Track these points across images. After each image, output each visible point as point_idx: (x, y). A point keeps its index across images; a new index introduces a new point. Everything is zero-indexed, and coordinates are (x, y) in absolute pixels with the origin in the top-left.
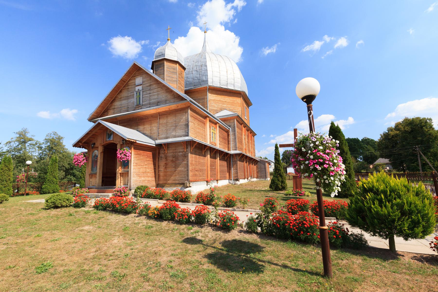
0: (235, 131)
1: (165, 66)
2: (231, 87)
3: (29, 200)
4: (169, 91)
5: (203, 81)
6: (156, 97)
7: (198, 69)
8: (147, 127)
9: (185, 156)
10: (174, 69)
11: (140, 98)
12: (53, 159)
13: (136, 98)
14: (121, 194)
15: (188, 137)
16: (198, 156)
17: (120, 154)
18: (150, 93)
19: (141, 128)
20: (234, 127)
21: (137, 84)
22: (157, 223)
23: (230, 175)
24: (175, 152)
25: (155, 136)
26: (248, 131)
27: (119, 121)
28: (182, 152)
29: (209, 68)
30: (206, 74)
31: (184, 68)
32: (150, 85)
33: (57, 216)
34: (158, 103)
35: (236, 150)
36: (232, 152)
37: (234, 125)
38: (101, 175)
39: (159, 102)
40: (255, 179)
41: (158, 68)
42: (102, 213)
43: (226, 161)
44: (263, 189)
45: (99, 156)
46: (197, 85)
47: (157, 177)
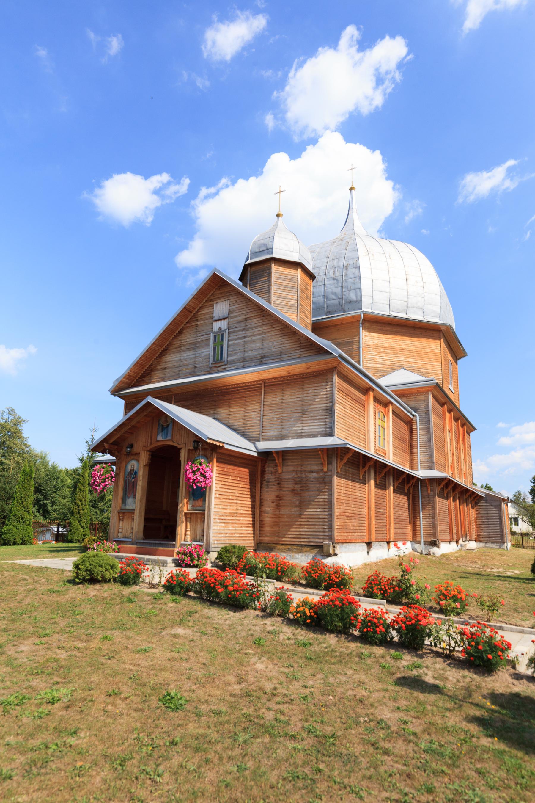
0: (428, 422)
1: (273, 275)
2: (416, 316)
3: (25, 557)
4: (287, 331)
5: (351, 302)
6: (258, 345)
7: (337, 274)
8: (236, 412)
9: (325, 483)
10: (291, 280)
11: (222, 347)
12: (24, 471)
13: (214, 348)
14: (192, 560)
15: (332, 438)
16: (350, 483)
17: (193, 472)
18: (245, 337)
19: (223, 412)
20: (427, 413)
21: (216, 318)
22: (316, 636)
23: (414, 530)
24: (301, 472)
25: (254, 432)
26: (456, 420)
27: (176, 395)
28: (317, 472)
29: (364, 273)
30: (357, 286)
31: (312, 277)
32: (246, 320)
33: (99, 600)
34: (262, 360)
35: (431, 468)
36: (421, 473)
37: (427, 406)
38: (143, 513)
39: (264, 357)
40: (472, 545)
41: (256, 278)
42: (186, 604)
43: (407, 494)
44: (509, 574)
45: (141, 473)
46: (334, 312)
47: (257, 525)
